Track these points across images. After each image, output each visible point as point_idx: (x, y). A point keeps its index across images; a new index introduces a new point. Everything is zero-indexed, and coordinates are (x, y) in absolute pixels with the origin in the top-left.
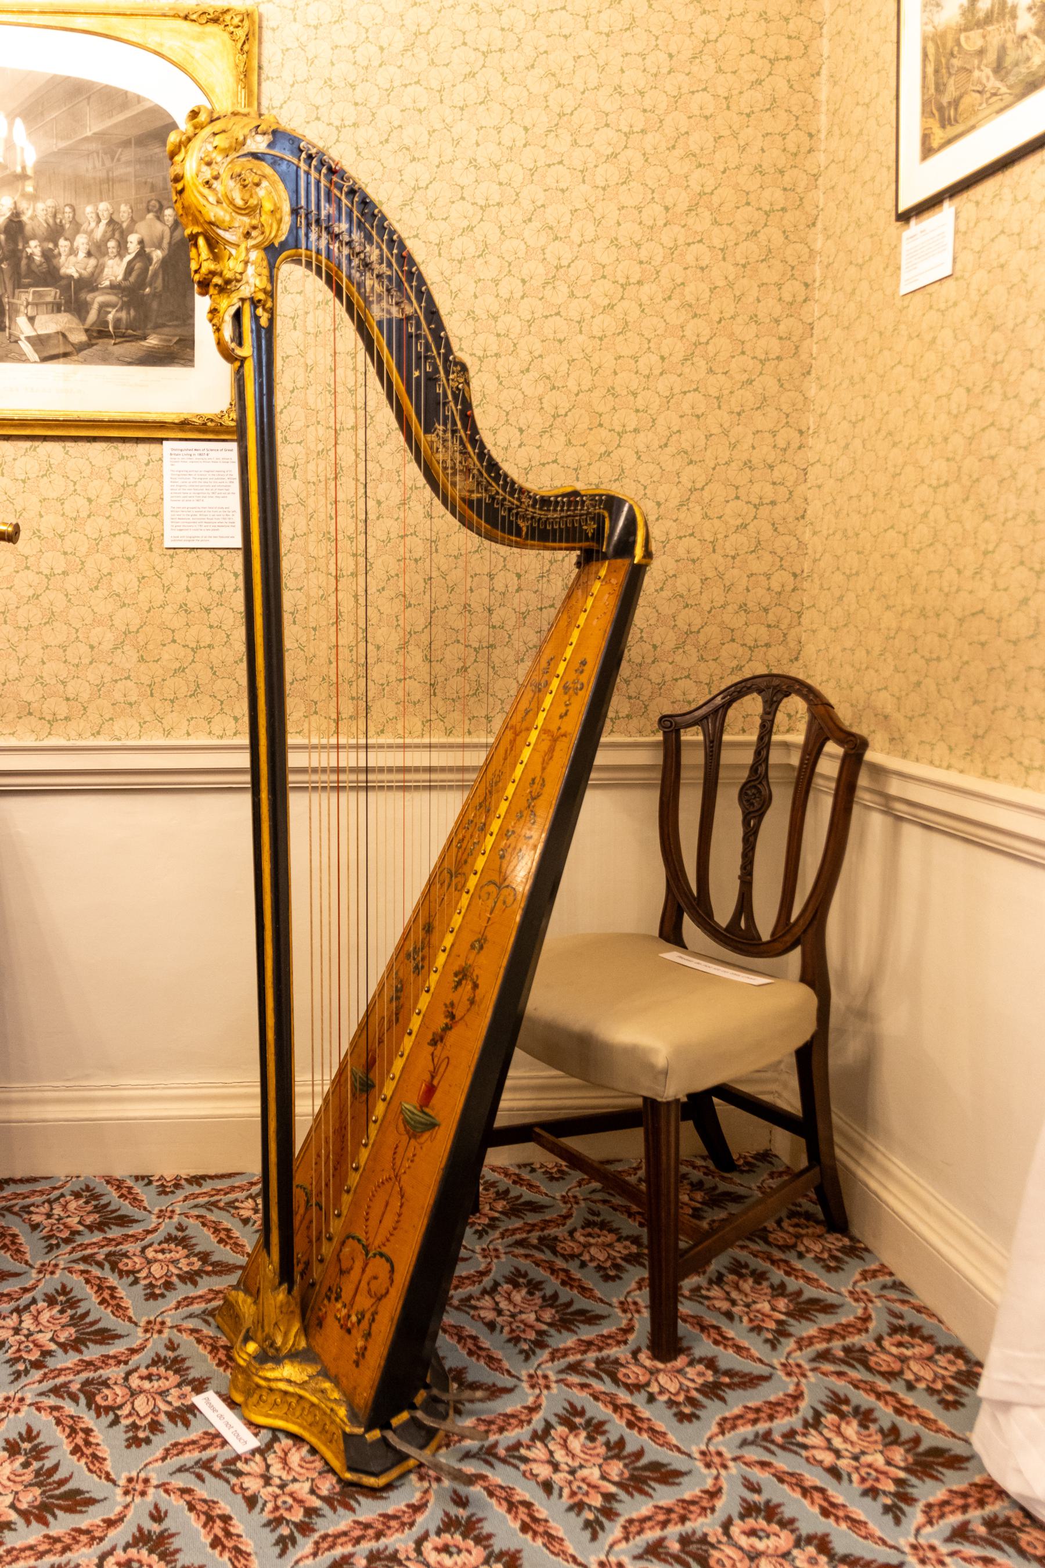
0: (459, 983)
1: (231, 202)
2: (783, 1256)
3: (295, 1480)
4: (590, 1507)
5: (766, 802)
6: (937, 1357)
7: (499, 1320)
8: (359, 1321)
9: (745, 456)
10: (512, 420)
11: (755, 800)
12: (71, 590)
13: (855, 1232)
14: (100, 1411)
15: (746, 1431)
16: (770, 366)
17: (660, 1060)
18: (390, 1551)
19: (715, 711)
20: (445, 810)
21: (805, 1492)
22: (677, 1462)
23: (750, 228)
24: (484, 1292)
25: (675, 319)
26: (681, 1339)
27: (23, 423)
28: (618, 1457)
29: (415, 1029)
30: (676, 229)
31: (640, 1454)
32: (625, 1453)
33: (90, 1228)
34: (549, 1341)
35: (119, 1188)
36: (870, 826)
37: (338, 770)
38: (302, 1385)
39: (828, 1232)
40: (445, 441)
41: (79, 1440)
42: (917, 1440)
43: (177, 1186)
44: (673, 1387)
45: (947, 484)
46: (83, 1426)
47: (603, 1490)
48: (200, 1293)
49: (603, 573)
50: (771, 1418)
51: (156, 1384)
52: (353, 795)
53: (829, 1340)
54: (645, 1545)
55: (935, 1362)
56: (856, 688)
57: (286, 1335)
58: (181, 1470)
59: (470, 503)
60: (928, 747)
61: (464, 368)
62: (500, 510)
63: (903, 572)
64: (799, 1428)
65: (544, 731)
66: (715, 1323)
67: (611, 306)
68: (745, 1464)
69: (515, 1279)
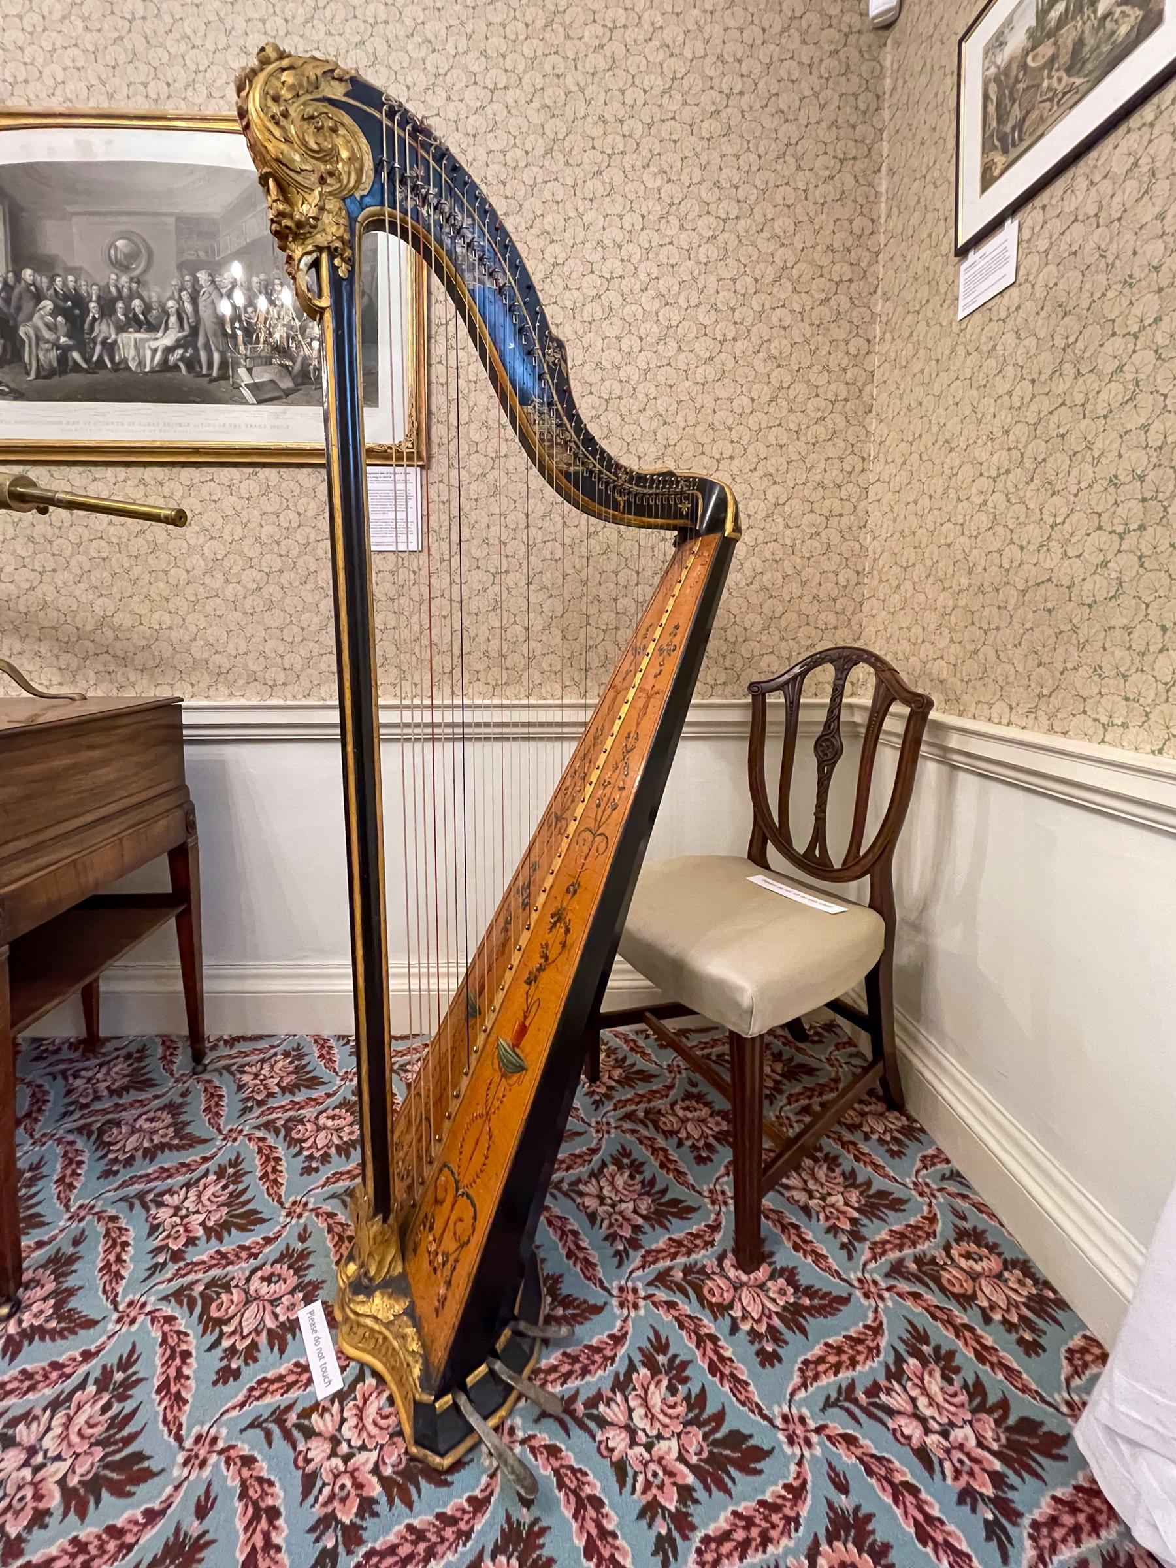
0: (554, 925)
1: (305, 144)
5: (838, 753)
6: (1006, 1274)
7: (601, 1210)
9: (818, 478)
10: (632, 449)
11: (828, 752)
12: (286, 584)
13: (910, 1108)
14: (292, 1142)
15: (828, 1382)
16: (839, 406)
17: (746, 1002)
19: (795, 678)
20: (556, 759)
22: (898, 1192)
23: (823, 296)
25: (761, 368)
27: (243, 452)
28: (696, 1422)
30: (764, 296)
31: (720, 1417)
32: (705, 1416)
33: (283, 1090)
36: (929, 772)
37: (433, 725)
38: (388, 1325)
39: (888, 1109)
40: (541, 413)
45: (1008, 472)
49: (696, 549)
52: (449, 745)
56: (912, 659)
59: (567, 475)
60: (986, 707)
61: (561, 346)
62: (597, 485)
63: (960, 557)
65: (640, 689)
66: (794, 1221)
69: (622, 1158)
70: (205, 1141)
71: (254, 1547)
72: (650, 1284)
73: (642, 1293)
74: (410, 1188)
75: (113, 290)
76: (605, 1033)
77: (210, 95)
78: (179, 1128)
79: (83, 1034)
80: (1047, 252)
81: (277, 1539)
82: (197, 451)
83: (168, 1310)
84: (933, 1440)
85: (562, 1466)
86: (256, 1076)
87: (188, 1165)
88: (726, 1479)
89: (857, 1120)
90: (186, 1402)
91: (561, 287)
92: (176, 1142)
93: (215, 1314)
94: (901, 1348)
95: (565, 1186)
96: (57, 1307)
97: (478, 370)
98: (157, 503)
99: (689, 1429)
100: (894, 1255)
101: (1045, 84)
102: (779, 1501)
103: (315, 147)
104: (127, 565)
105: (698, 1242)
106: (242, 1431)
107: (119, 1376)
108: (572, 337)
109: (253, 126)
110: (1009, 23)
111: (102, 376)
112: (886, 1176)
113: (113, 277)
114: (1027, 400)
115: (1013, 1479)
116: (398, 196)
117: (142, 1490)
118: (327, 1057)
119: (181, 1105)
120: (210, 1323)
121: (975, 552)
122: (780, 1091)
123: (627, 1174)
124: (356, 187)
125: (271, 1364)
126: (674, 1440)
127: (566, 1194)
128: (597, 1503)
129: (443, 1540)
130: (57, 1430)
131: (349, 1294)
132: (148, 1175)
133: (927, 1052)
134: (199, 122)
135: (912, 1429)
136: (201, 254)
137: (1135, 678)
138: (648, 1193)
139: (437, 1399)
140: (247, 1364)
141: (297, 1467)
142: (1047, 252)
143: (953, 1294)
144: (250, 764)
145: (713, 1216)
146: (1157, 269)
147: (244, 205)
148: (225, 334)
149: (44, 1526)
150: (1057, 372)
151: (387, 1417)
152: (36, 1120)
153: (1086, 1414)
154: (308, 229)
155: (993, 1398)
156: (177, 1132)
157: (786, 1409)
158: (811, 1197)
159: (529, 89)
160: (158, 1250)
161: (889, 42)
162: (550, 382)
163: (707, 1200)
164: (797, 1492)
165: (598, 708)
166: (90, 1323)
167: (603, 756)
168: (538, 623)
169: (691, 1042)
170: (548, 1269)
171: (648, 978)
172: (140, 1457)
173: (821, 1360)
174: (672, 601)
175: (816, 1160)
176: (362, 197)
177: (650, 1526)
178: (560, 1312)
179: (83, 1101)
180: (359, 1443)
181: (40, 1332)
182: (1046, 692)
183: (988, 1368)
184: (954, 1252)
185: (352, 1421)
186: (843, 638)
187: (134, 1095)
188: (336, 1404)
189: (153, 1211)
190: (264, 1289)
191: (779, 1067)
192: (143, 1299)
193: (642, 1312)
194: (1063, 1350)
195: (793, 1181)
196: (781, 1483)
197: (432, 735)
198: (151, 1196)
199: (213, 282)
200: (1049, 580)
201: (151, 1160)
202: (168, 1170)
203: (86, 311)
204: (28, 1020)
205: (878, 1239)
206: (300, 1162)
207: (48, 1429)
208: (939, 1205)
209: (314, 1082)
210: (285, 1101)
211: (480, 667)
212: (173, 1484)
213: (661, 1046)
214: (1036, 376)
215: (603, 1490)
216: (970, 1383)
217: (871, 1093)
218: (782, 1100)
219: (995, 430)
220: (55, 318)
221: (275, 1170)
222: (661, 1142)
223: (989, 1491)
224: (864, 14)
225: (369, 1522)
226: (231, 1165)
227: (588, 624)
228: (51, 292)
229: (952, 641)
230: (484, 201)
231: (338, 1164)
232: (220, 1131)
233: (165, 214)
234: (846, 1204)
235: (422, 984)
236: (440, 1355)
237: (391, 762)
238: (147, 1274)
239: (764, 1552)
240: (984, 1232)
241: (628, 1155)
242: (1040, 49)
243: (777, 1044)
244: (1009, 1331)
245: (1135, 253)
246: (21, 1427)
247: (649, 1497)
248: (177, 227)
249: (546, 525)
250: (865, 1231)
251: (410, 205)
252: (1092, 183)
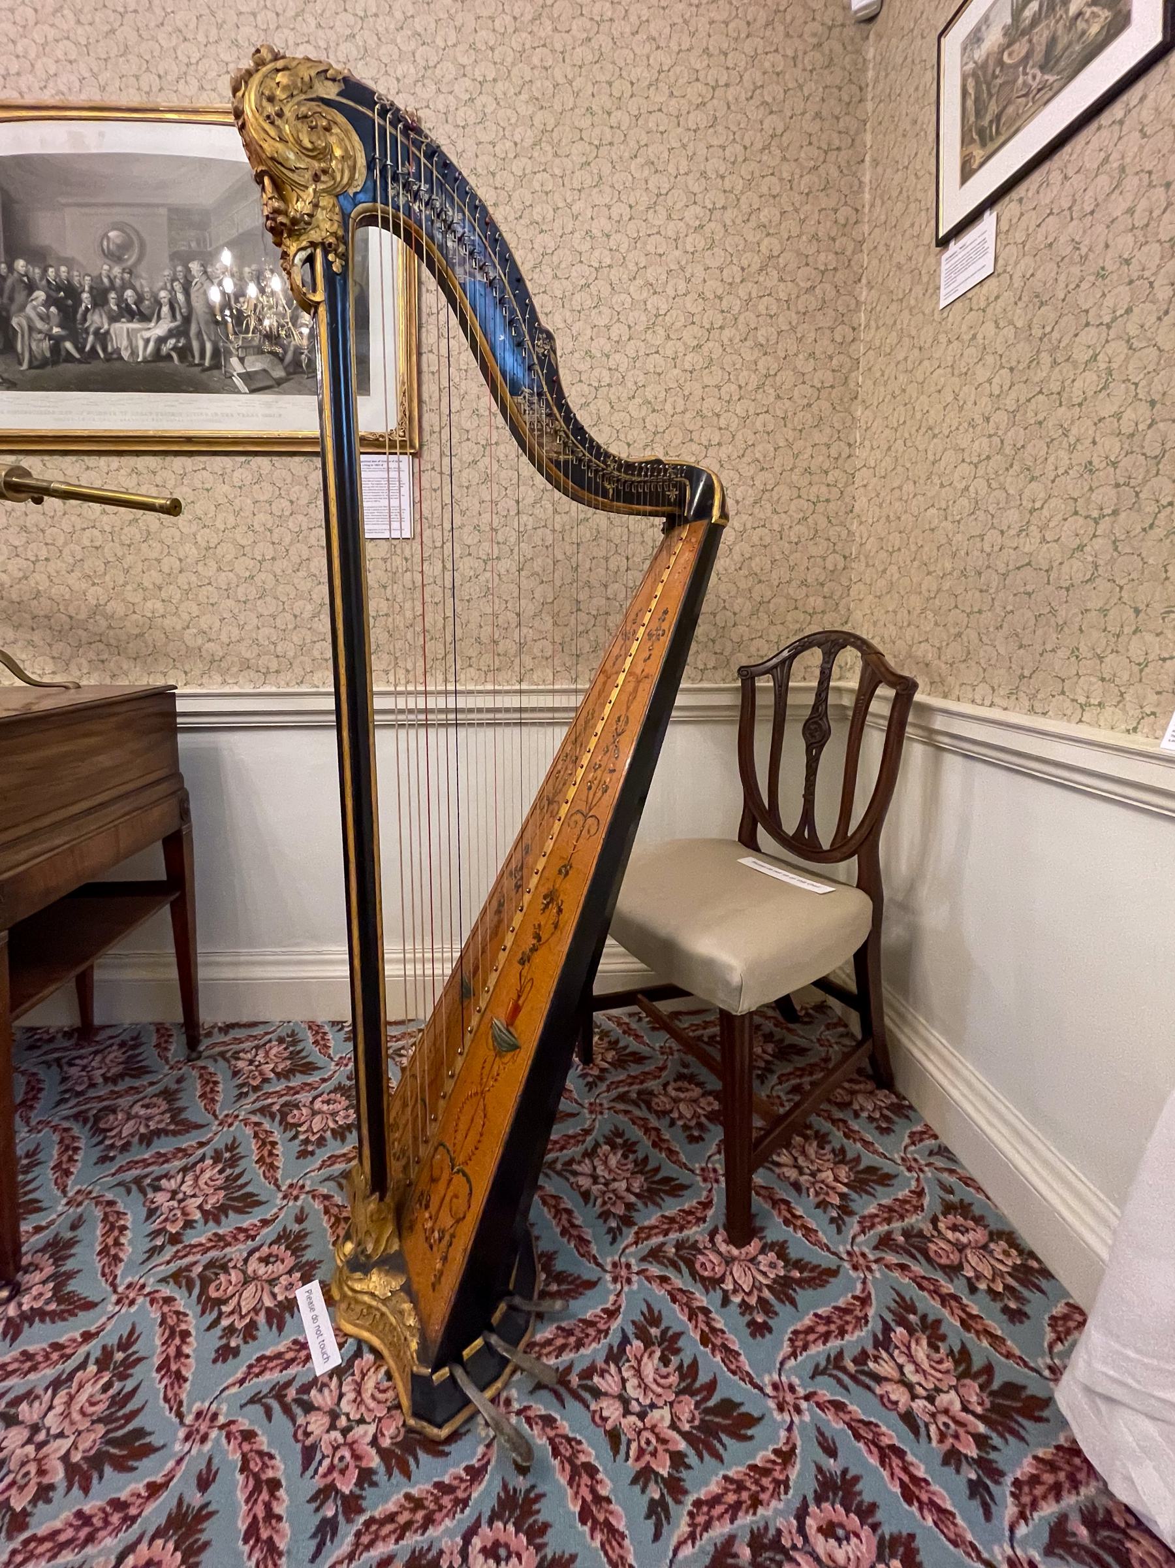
0: (547, 906)
1: (299, 142)
5: (825, 735)
6: (992, 1246)
8: (440, 1239)
10: (622, 436)
12: (279, 572)
13: (900, 1088)
15: (818, 1351)
17: (735, 979)
19: (783, 662)
20: (548, 743)
22: (887, 1167)
26: (755, 1216)
27: (236, 441)
28: (688, 1391)
29: (509, 945)
31: (711, 1386)
32: (697, 1385)
36: (915, 754)
37: (426, 711)
38: (384, 1301)
40: (531, 403)
47: (671, 1447)
49: (684, 535)
52: (442, 731)
54: (711, 1549)
55: (991, 1252)
56: (898, 642)
57: (377, 1242)
60: (969, 688)
61: (550, 337)
62: (586, 472)
67: (699, 346)
69: (616, 1139)
71: (255, 1517)
72: (643, 1259)
73: (635, 1269)
74: (406, 1168)
75: (106, 280)
76: (599, 1016)
77: (202, 88)
78: (175, 1114)
79: (77, 1022)
80: (1024, 244)
81: (278, 1509)
82: (189, 440)
83: (166, 1291)
84: (919, 1405)
85: (557, 1435)
86: (251, 1062)
87: (184, 1150)
88: (718, 1446)
89: (847, 1098)
90: (186, 1380)
91: (550, 276)
92: (172, 1127)
93: (213, 1294)
94: (889, 1317)
95: (559, 1166)
96: (56, 1290)
97: (467, 358)
98: (147, 492)
99: (682, 1398)
100: (882, 1229)
101: (1020, 81)
102: (769, 1465)
103: (309, 146)
104: (120, 554)
105: (690, 1218)
106: (242, 1407)
107: (119, 1356)
108: (562, 325)
109: (248, 125)
110: (986, 20)
111: (94, 366)
112: (875, 1152)
113: (106, 267)
114: (1006, 388)
115: (996, 1440)
116: (391, 193)
117: (145, 1464)
118: (321, 1042)
119: (177, 1091)
120: (209, 1304)
121: (959, 537)
122: (772, 1072)
123: (620, 1153)
124: (349, 184)
125: (271, 1343)
126: (667, 1408)
127: (559, 1174)
128: (591, 1470)
129: (441, 1508)
130: (59, 1409)
131: (346, 1271)
132: (144, 1160)
133: (916, 1032)
134: (191, 114)
135: (899, 1394)
136: (193, 245)
137: (1110, 659)
138: (641, 1172)
139: (434, 1372)
140: (246, 1342)
141: (297, 1441)
142: (1024, 244)
143: (940, 1265)
144: (242, 749)
145: (705, 1193)
146: (1127, 262)
147: (235, 195)
148: (217, 322)
149: (48, 1501)
150: (1035, 361)
151: (384, 1391)
152: (32, 1107)
153: (1066, 1377)
154: (302, 225)
155: (978, 1363)
156: (173, 1118)
157: (776, 1377)
158: (801, 1173)
159: (518, 205)
160: (156, 1233)
161: (872, 36)
162: (540, 373)
163: (699, 1178)
164: (786, 1456)
165: (588, 693)
166: (89, 1305)
167: (594, 740)
168: (529, 608)
169: (684, 1023)
170: (542, 1246)
171: (642, 961)
172: (140, 1433)
173: (810, 1330)
174: (660, 587)
175: (806, 1138)
176: (356, 194)
177: (643, 1491)
178: (554, 1287)
179: (79, 1088)
180: (358, 1417)
181: (40, 1314)
182: (1027, 673)
183: (972, 1335)
184: (941, 1226)
185: (351, 1396)
186: (830, 622)
187: (128, 1082)
188: (335, 1379)
189: (150, 1195)
190: (262, 1270)
191: (770, 1048)
192: (142, 1281)
193: (635, 1287)
194: (1046, 1317)
195: (784, 1158)
196: (771, 1448)
197: (425, 721)
198: (148, 1181)
199: (205, 272)
200: (1029, 564)
201: (148, 1145)
202: (164, 1155)
203: (78, 301)
204: (27, 1005)
205: (866, 1213)
206: (296, 1146)
207: (51, 1408)
208: (927, 1179)
209: (309, 1068)
210: (280, 1086)
211: (472, 652)
212: (175, 1456)
213: (653, 1029)
214: (1014, 364)
215: (597, 1457)
216: (956, 1349)
217: (860, 1071)
218: (774, 1079)
219: (976, 417)
220: (48, 309)
221: (271, 1154)
222: (654, 1122)
223: (973, 1452)
224: (847, 8)
225: (369, 1492)
226: (228, 1149)
227: (579, 610)
228: (44, 282)
229: (936, 624)
230: (474, 196)
231: (335, 1147)
232: (216, 1117)
233: (158, 206)
234: (836, 1179)
235: (416, 969)
236: (437, 1328)
237: (386, 747)
239: (754, 1514)
240: (971, 1204)
241: (620, 1135)
242: (1016, 46)
243: (768, 1026)
244: (994, 1300)
245: (1107, 246)
246: (24, 1406)
247: (642, 1464)
248: (170, 219)
249: (537, 512)
250: (853, 1206)
251: (401, 201)
252: (1066, 178)
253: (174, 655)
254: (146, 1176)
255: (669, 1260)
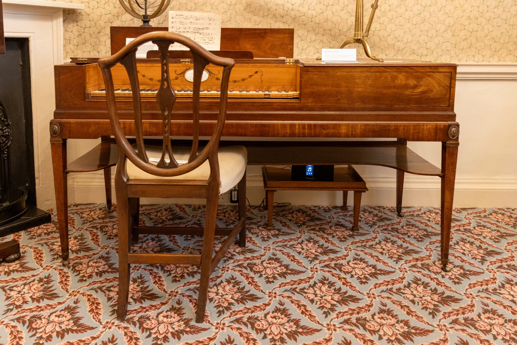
2: (436, 277)
3: (226, 294)
4: (326, 308)
6: (505, 324)
14: (144, 330)
18: (256, 316)
21: (402, 307)
22: (359, 296)
24: (290, 213)
33: (169, 220)
34: (319, 257)
35: (180, 208)
41: (157, 280)
42: (443, 293)
43: (199, 208)
44: (360, 273)
46: (135, 336)
48: (195, 280)
50: (393, 284)
51: (169, 320)
53: (416, 262)
58: (189, 290)
64: (402, 288)
68: (382, 297)
70: (92, 328)
78: (76, 321)
156: (21, 266)
187: (46, 302)
193: (225, 331)
198: (8, 287)
202: (16, 279)
238: (4, 312)
253: (383, 47)
254: (104, 286)
255: (463, 324)
